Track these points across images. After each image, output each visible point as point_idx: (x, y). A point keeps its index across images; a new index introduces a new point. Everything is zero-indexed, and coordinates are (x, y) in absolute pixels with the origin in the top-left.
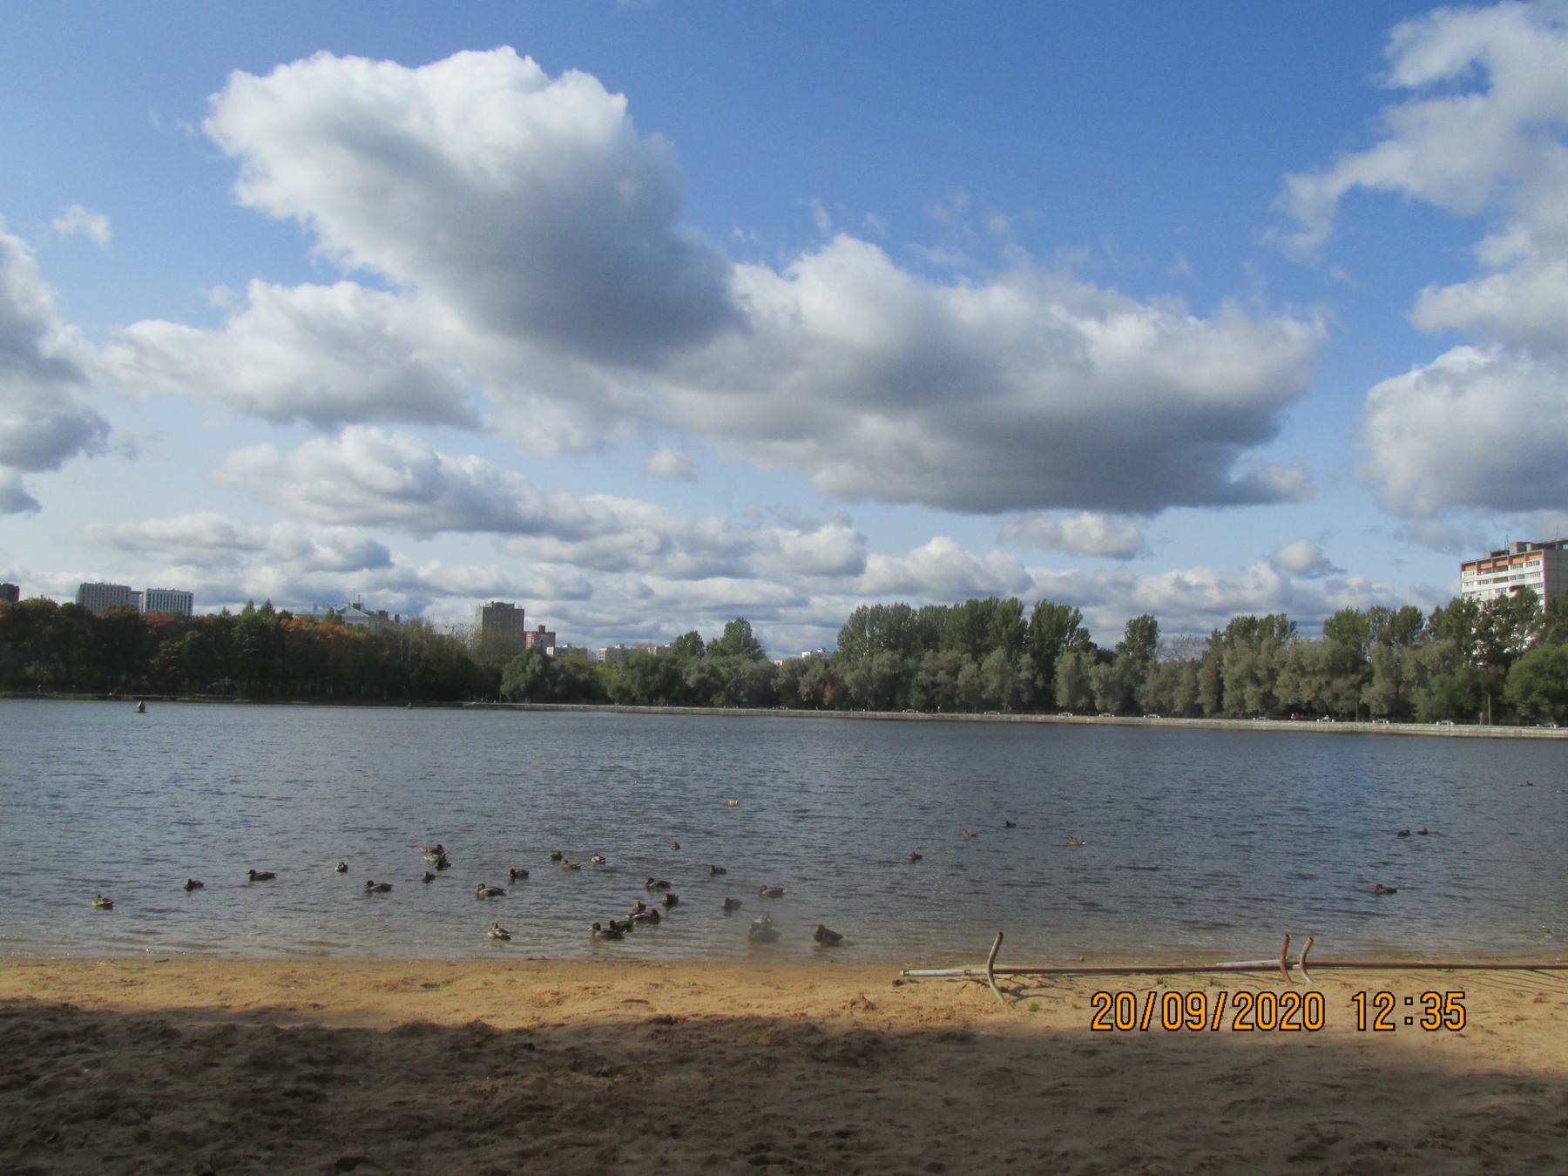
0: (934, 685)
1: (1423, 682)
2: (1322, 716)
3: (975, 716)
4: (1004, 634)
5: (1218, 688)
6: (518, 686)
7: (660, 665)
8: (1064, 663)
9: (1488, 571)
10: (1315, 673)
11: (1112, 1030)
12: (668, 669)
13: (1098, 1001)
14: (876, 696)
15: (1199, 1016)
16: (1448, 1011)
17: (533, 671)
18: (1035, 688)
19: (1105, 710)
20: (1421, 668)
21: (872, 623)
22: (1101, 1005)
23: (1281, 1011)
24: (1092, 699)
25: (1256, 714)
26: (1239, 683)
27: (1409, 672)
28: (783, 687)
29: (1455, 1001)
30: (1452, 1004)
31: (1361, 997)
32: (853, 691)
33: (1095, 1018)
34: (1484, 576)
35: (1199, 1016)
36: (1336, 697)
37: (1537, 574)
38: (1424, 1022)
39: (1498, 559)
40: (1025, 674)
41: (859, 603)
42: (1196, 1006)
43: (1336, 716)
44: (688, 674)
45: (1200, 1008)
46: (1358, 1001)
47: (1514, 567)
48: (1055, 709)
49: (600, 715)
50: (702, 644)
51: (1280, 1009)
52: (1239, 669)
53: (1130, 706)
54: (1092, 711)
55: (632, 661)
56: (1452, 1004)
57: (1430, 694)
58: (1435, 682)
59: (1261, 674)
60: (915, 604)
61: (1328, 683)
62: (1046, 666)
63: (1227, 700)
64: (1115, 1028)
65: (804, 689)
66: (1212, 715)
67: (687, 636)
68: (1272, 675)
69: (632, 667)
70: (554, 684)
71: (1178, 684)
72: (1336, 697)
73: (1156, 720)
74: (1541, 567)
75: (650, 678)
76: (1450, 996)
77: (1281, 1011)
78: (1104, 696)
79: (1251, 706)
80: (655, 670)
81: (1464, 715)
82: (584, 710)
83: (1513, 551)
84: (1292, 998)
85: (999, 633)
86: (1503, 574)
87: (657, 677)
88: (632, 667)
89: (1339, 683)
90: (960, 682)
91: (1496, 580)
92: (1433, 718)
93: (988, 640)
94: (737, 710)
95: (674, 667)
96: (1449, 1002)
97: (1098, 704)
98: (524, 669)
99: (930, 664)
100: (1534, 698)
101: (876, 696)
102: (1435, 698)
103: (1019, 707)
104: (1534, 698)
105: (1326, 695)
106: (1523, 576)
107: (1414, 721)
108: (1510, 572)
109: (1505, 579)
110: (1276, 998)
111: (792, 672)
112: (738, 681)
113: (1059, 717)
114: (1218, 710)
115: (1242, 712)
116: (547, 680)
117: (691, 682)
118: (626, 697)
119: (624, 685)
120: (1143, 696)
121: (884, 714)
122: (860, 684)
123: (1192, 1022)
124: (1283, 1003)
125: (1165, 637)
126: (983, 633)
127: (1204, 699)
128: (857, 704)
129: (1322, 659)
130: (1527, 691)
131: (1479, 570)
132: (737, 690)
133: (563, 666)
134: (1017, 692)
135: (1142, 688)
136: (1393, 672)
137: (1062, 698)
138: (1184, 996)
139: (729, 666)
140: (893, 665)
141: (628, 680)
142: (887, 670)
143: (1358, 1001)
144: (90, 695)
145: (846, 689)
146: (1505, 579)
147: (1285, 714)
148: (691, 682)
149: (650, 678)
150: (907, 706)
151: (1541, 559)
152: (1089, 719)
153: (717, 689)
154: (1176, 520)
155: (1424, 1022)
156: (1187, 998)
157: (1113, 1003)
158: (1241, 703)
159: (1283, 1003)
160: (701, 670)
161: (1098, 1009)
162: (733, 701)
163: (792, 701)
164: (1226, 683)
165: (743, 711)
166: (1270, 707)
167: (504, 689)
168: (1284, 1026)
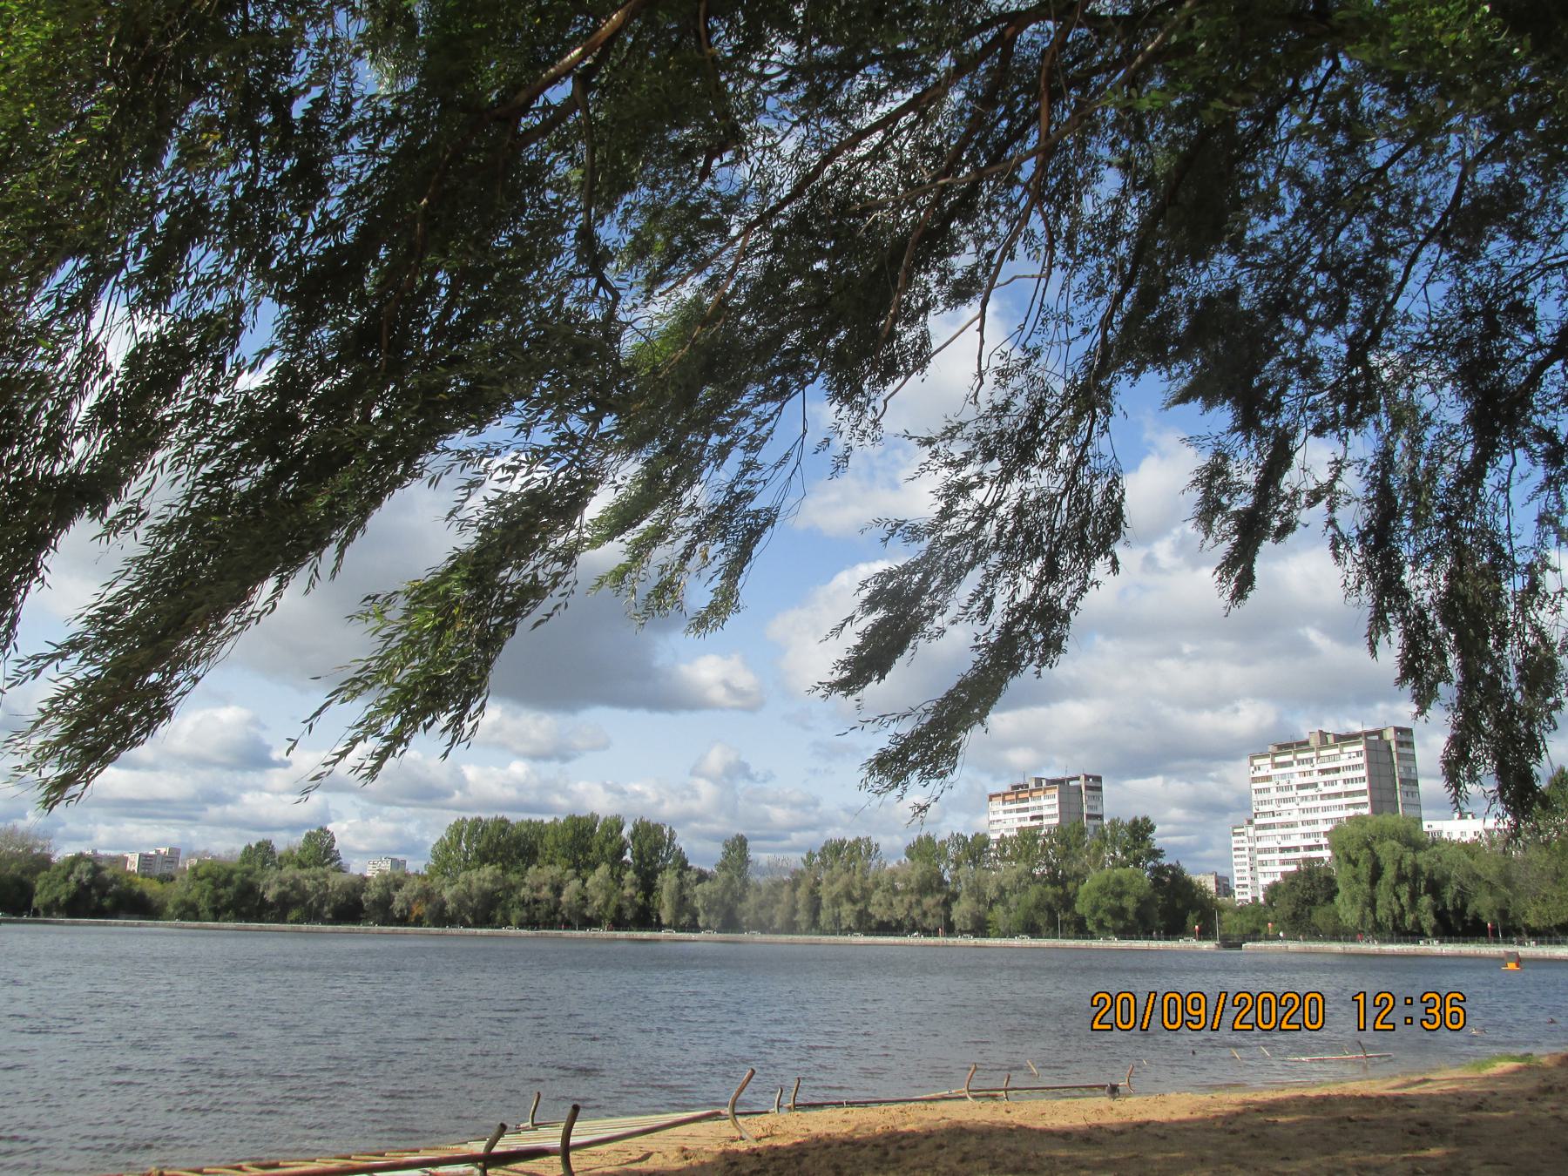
0: (536, 901)
2: (911, 932)
3: (578, 933)
4: (607, 851)
5: (815, 907)
6: (57, 899)
7: (234, 877)
8: (667, 882)
9: (1012, 802)
10: (905, 892)
12: (243, 881)
14: (474, 912)
17: (79, 881)
18: (636, 905)
19: (707, 927)
20: (1002, 890)
21: (470, 835)
23: (1281, 1011)
24: (695, 916)
25: (849, 931)
26: (836, 902)
27: (991, 892)
28: (374, 902)
31: (1361, 997)
32: (450, 907)
34: (1008, 806)
36: (925, 914)
37: (1362, 793)
39: (1019, 791)
40: (628, 891)
41: (452, 818)
43: (927, 932)
44: (268, 887)
47: (1034, 799)
48: (659, 926)
49: (160, 927)
50: (272, 853)
52: (838, 887)
53: (730, 923)
54: (693, 927)
55: (201, 872)
57: (1008, 911)
58: (1013, 900)
59: (856, 893)
60: (514, 818)
61: (919, 903)
62: (648, 884)
63: (824, 917)
65: (398, 905)
66: (807, 932)
67: (259, 845)
68: (866, 894)
69: (201, 879)
70: (103, 895)
71: (778, 902)
72: (925, 914)
73: (758, 937)
74: (1056, 801)
75: (221, 891)
77: (1281, 1011)
78: (707, 913)
79: (849, 920)
80: (228, 882)
81: (1032, 930)
82: (139, 925)
83: (1032, 785)
85: (602, 849)
87: (230, 890)
88: (201, 879)
89: (929, 901)
90: (563, 899)
91: (1018, 810)
92: (1010, 934)
93: (591, 856)
94: (320, 926)
95: (250, 879)
97: (701, 922)
98: (66, 879)
99: (537, 878)
100: (1100, 914)
101: (474, 912)
102: (1013, 915)
103: (618, 923)
104: (1100, 914)
105: (916, 913)
106: (1040, 808)
107: (988, 936)
108: (1031, 804)
109: (1026, 810)
111: (385, 885)
112: (324, 895)
113: (663, 934)
114: (814, 925)
115: (837, 928)
116: (93, 891)
117: (270, 895)
118: (189, 911)
119: (189, 898)
120: (743, 914)
121: (485, 931)
122: (461, 903)
125: (760, 856)
126: (586, 849)
127: (802, 917)
128: (452, 922)
129: (913, 879)
130: (1095, 909)
131: (1004, 801)
132: (321, 905)
133: (115, 876)
134: (619, 909)
135: (743, 906)
136: (977, 892)
137: (666, 916)
139: (315, 879)
140: (495, 880)
141: (196, 892)
142: (488, 886)
145: (444, 904)
146: (1026, 810)
147: (885, 928)
148: (270, 895)
149: (221, 891)
150: (507, 923)
151: (1055, 792)
152: (693, 936)
153: (295, 904)
154: (599, 719)
157: (1113, 1004)
158: (837, 920)
160: (282, 883)
162: (313, 915)
163: (379, 917)
164: (824, 902)
165: (329, 928)
166: (868, 924)
167: (37, 901)
168: (1284, 1026)
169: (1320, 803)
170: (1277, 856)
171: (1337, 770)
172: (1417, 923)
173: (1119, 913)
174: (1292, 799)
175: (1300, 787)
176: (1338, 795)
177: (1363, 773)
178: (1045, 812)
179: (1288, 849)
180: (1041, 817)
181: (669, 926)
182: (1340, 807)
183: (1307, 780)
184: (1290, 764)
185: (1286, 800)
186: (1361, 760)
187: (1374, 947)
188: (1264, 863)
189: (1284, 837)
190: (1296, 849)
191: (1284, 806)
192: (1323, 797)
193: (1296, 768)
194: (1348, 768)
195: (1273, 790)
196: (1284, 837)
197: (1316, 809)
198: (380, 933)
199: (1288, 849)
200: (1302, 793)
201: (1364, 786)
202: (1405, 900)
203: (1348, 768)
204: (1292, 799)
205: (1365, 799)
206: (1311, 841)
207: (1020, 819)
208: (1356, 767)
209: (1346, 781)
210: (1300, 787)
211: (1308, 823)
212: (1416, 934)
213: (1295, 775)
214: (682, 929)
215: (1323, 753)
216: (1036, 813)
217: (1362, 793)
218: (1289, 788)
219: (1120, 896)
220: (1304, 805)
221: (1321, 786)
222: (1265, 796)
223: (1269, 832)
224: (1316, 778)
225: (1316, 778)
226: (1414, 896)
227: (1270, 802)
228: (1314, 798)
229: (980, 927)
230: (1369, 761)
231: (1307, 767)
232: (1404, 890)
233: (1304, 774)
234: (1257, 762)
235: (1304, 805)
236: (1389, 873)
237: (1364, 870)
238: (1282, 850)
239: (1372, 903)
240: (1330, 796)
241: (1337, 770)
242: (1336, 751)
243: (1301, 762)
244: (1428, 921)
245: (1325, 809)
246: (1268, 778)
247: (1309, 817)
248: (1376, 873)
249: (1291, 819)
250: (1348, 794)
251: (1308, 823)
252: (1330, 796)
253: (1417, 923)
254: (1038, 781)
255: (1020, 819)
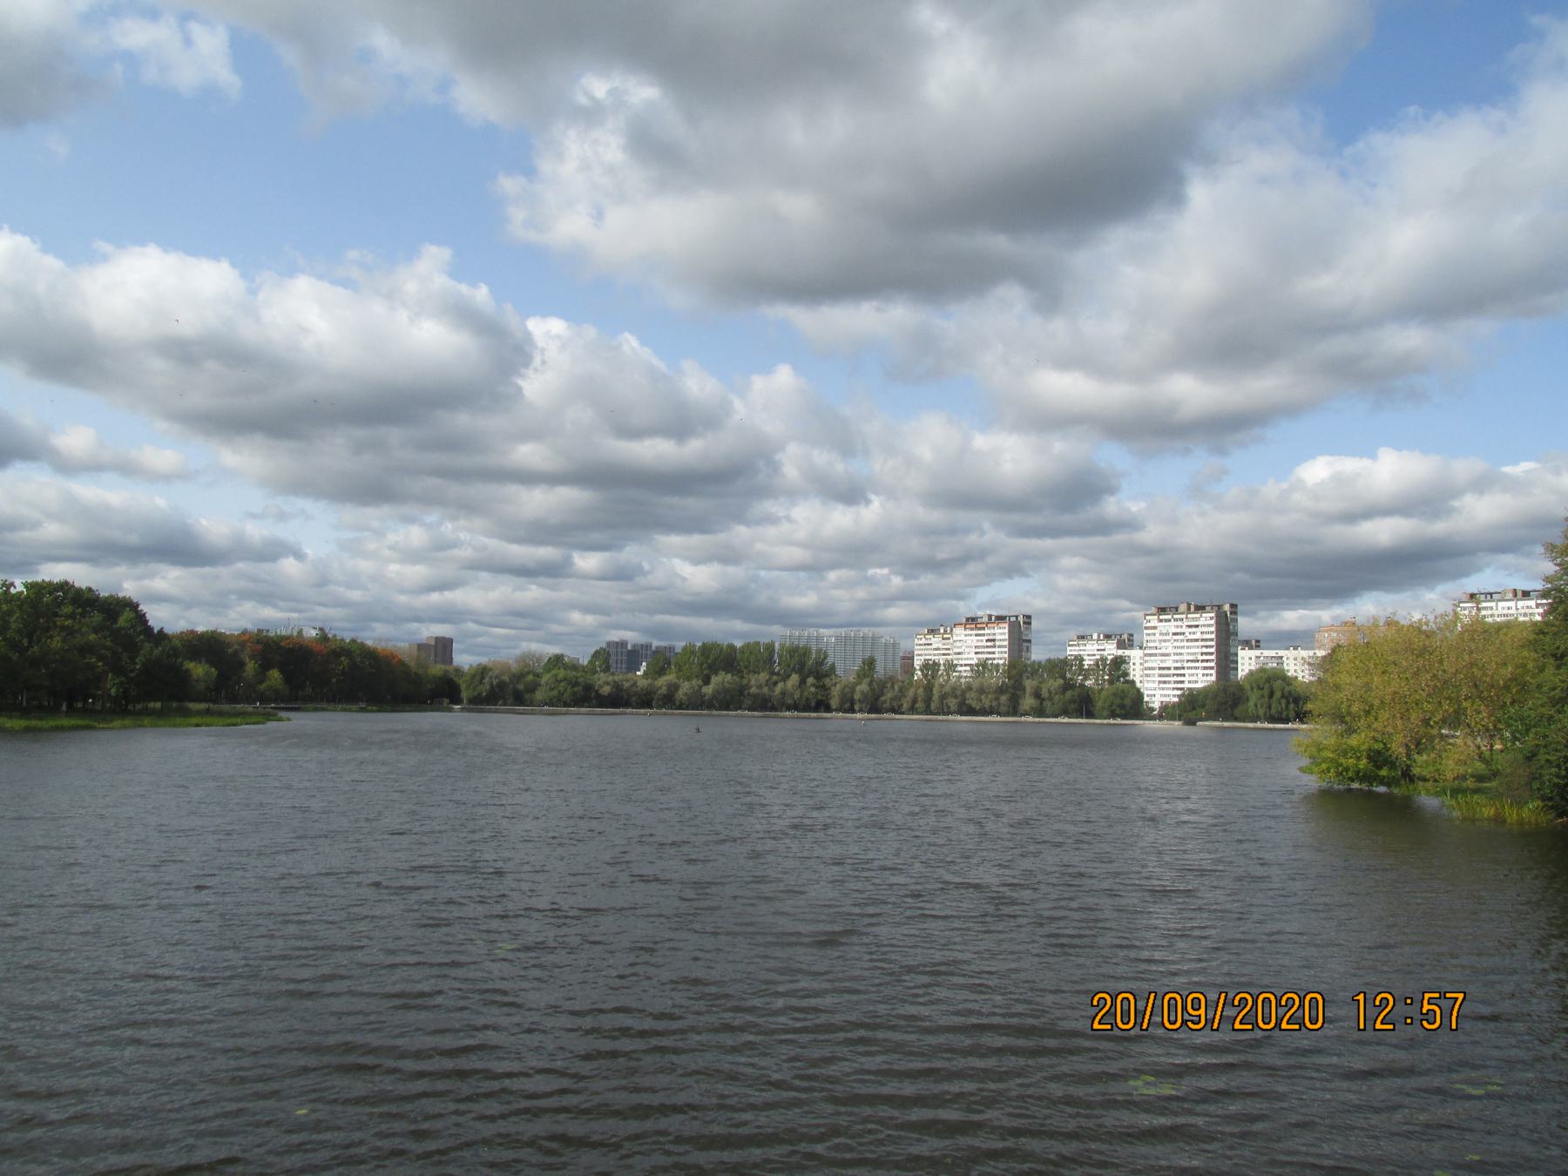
1: (1051, 699)
5: (928, 700)
6: (479, 695)
9: (972, 629)
11: (1112, 1030)
13: (1239, 1002)
15: (1199, 1016)
16: (1424, 1011)
22: (1384, 1005)
29: (1431, 1001)
30: (1429, 1004)
31: (1361, 997)
33: (1094, 1018)
34: (968, 632)
35: (1199, 1016)
37: (1212, 640)
38: (1425, 1023)
42: (1196, 1007)
43: (999, 714)
45: (1200, 1008)
46: (1358, 1001)
51: (1279, 1009)
54: (853, 711)
56: (1429, 1004)
57: (1053, 704)
64: (1115, 1028)
69: (561, 681)
74: (1006, 631)
75: (576, 689)
76: (1427, 996)
84: (1386, 998)
86: (982, 632)
88: (561, 681)
91: (976, 635)
96: (1425, 1002)
97: (857, 707)
108: (987, 631)
109: (984, 635)
110: (1276, 998)
123: (1193, 1022)
124: (1283, 1003)
131: (965, 629)
138: (1279, 995)
143: (1358, 1001)
144: (374, 708)
146: (984, 635)
150: (740, 708)
155: (1425, 1023)
156: (1304, 998)
159: (1283, 1003)
161: (1098, 1009)
169: (1185, 644)
170: (1157, 672)
171: (1197, 626)
172: (1287, 715)
173: (1122, 706)
174: (1169, 641)
175: (1174, 634)
176: (1197, 640)
177: (1213, 629)
178: (998, 637)
179: (1163, 668)
180: (994, 640)
181: (837, 710)
182: (1198, 647)
183: (1178, 630)
184: (1170, 620)
185: (1165, 641)
186: (1212, 622)
187: (1066, 720)
188: (1147, 675)
189: (1162, 661)
190: (1169, 668)
191: (1163, 644)
192: (1187, 640)
193: (1173, 623)
194: (1204, 626)
195: (1157, 635)
196: (1162, 661)
197: (1183, 647)
198: (799, 718)
199: (1163, 668)
200: (1175, 637)
201: (1213, 636)
202: (1284, 706)
203: (1204, 626)
204: (1169, 641)
205: (1213, 643)
206: (1179, 665)
207: (978, 641)
208: (1209, 625)
209: (1202, 633)
210: (1174, 634)
211: (1177, 654)
212: (1287, 721)
213: (1171, 627)
214: (846, 711)
215: (1189, 616)
216: (991, 637)
217: (1212, 640)
218: (1167, 634)
219: (1122, 699)
220: (1176, 644)
221: (1187, 634)
222: (1152, 638)
223: (1153, 658)
224: (1184, 629)
225: (1184, 629)
226: (1288, 703)
227: (1155, 641)
228: (1182, 641)
229: (1040, 712)
230: (1217, 623)
231: (1180, 623)
232: (1284, 701)
233: (1177, 627)
234: (1148, 618)
235: (1176, 644)
236: (1278, 694)
237: (1266, 692)
238: (1160, 668)
239: (1270, 708)
240: (1192, 640)
241: (1197, 626)
242: (1198, 615)
243: (1176, 620)
244: (1292, 714)
245: (1188, 647)
246: (1155, 628)
247: (1178, 651)
248: (1271, 694)
249: (1167, 652)
250: (1202, 640)
251: (1177, 654)
252: (1192, 640)
253: (1287, 715)
254: (990, 617)
255: (978, 641)
